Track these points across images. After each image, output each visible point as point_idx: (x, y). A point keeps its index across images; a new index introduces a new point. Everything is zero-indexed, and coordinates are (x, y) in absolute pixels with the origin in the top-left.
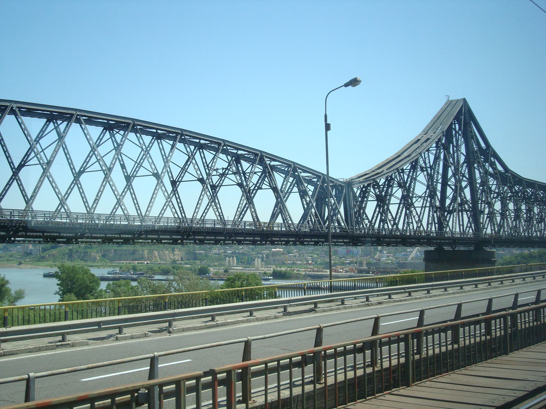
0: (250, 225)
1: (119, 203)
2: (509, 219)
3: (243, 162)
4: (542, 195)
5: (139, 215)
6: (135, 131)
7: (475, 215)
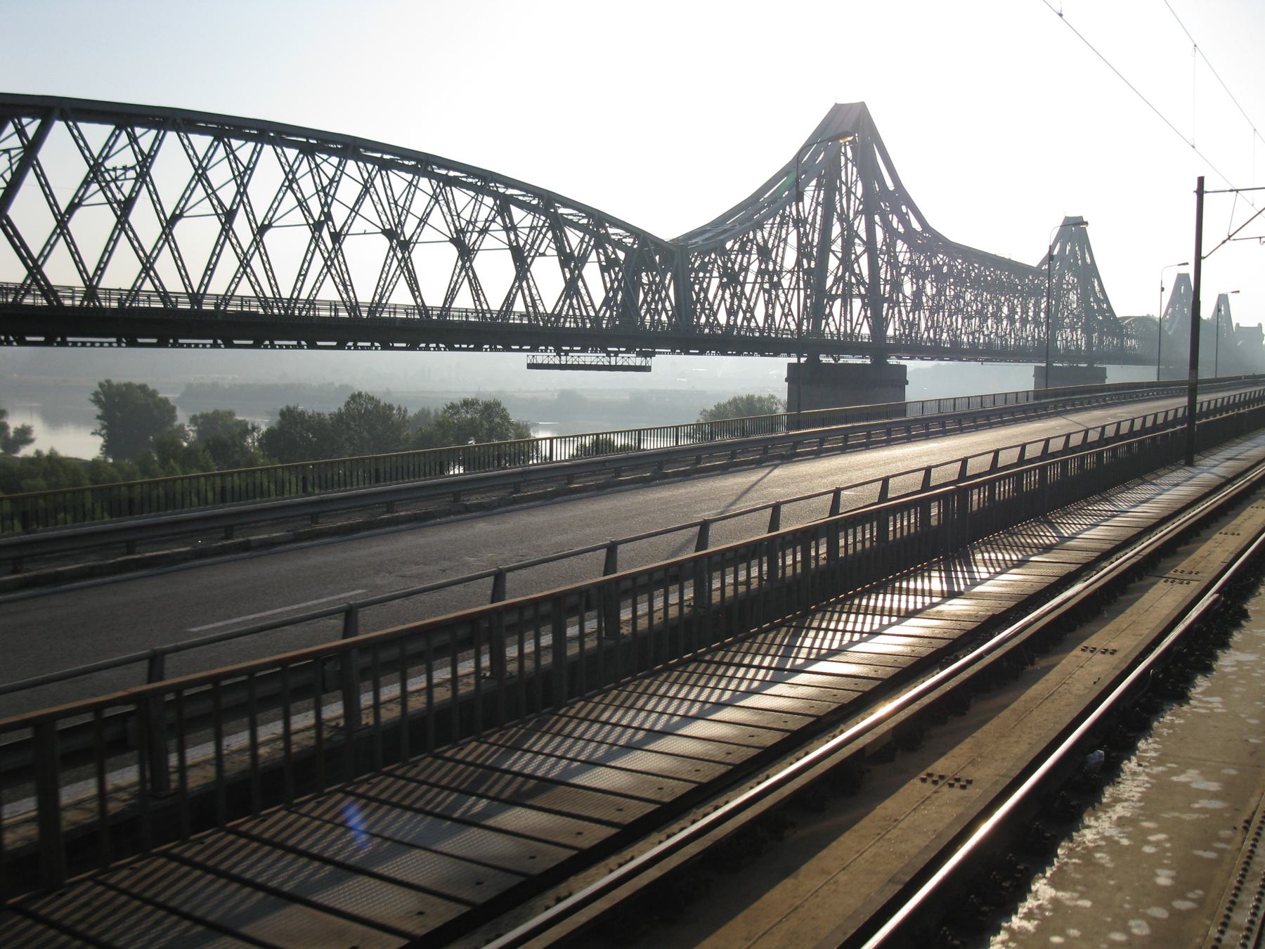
0: (521, 316)
1: (148, 267)
2: (902, 309)
3: (513, 208)
4: (959, 267)
5: (157, 290)
6: (273, 142)
7: (873, 301)
